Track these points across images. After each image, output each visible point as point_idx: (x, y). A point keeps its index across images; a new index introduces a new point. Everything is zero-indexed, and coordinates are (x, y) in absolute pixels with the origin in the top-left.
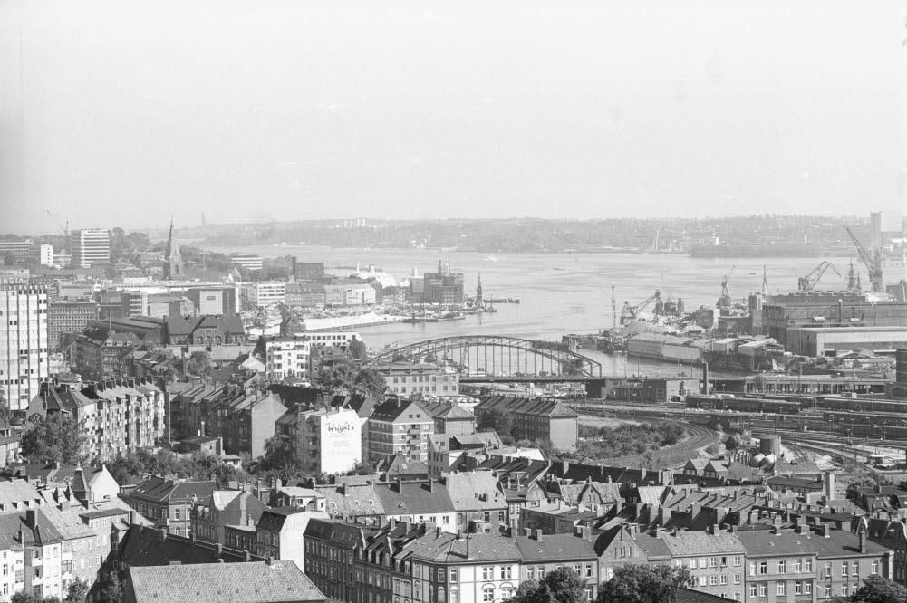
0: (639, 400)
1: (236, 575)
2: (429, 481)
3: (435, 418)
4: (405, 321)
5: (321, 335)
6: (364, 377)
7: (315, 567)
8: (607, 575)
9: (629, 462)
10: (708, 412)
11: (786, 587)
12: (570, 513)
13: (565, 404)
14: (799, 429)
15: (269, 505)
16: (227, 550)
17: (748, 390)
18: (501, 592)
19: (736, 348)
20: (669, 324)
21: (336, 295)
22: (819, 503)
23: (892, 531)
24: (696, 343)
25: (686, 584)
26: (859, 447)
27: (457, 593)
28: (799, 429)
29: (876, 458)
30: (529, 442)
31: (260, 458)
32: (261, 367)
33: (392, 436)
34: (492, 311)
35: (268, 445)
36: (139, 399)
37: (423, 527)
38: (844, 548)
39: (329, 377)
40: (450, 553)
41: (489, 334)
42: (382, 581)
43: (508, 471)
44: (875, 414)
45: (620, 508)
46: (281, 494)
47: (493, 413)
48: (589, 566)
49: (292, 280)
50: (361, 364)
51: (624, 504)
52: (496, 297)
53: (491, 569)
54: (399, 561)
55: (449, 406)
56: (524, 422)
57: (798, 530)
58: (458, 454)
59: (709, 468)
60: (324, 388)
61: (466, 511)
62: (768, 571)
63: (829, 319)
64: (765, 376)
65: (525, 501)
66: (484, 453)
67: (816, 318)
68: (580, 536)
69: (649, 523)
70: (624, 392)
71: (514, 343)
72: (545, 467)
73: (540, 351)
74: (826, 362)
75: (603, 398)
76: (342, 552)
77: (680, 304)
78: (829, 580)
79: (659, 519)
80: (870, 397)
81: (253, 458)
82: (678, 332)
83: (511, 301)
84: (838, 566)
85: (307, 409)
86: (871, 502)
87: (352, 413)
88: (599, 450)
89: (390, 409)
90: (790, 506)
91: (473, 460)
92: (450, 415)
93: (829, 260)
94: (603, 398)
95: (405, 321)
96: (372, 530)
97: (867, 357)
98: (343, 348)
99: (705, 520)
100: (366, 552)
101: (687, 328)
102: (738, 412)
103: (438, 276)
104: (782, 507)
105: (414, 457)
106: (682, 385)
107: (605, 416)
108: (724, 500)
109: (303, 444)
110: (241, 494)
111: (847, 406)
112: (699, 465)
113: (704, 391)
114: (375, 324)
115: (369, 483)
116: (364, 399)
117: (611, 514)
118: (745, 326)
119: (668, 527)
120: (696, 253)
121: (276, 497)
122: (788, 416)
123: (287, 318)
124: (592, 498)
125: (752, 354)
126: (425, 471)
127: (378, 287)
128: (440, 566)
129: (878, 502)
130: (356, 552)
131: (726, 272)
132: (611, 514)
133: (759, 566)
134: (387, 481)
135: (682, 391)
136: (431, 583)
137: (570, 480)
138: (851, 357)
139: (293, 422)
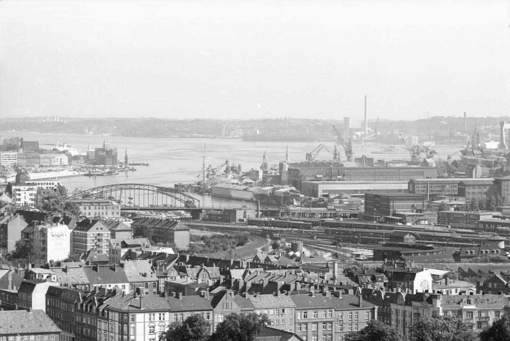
0: (221, 221)
1: (5, 317)
2: (112, 265)
3: (110, 230)
4: (85, 175)
5: (40, 182)
6: (68, 206)
7: (51, 311)
8: (220, 319)
9: (220, 255)
10: (260, 228)
11: (318, 326)
12: (193, 284)
13: (184, 223)
14: (312, 238)
15: (24, 278)
16: (4, 303)
17: (281, 216)
18: (159, 328)
19: (273, 192)
20: (234, 178)
21: (45, 160)
22: (331, 279)
23: (375, 295)
24: (251, 189)
25: (266, 324)
26: (347, 248)
27: (134, 328)
28: (312, 238)
29: (356, 255)
30: (163, 244)
31: (12, 251)
32: (9, 200)
33: (86, 240)
34: (133, 170)
35: (17, 244)
37: (115, 291)
38: (350, 304)
39: (50, 206)
40: (130, 306)
41: (138, 183)
42: (91, 322)
43: (157, 260)
44: (354, 230)
45: (222, 281)
46: (32, 272)
47: (142, 227)
48: (208, 314)
49: (21, 151)
50: (65, 199)
51: (224, 279)
52: (135, 162)
53: (154, 315)
54: (101, 310)
55: (118, 224)
56: (159, 232)
57: (324, 294)
58: (126, 250)
59: (267, 259)
60: (48, 212)
61: (135, 282)
62: (308, 317)
63: (325, 176)
64: (291, 208)
65: (167, 277)
66: (141, 250)
67: (318, 176)
68: (203, 296)
69: (240, 291)
70: (213, 216)
71: (151, 188)
72: (176, 258)
73: (166, 192)
74: (324, 201)
75: (201, 219)
76: (68, 305)
77: (239, 167)
78: (341, 322)
79: (244, 289)
80: (351, 220)
81: (9, 251)
82: (239, 183)
83: (144, 165)
84: (347, 314)
85: (40, 224)
86: (361, 279)
87: (65, 227)
88: (201, 249)
89: (86, 225)
90: (316, 281)
91: (135, 254)
92: (118, 228)
93: (322, 143)
94: (201, 219)
95: (85, 175)
96: (86, 292)
97: (347, 198)
98: (55, 190)
99: (271, 289)
100: (82, 305)
101: (245, 181)
102: (277, 228)
103: (103, 150)
104: (312, 281)
105: (99, 252)
106: (245, 213)
107: (203, 230)
108: (281, 277)
109: (37, 244)
110: (8, 272)
111: (338, 225)
112: (262, 257)
113: (257, 216)
114: (68, 177)
115: (81, 266)
116: (71, 219)
117: (217, 284)
118: (277, 180)
119: (250, 292)
120: (246, 138)
121: (28, 274)
122: (305, 230)
123: (20, 172)
124: (205, 275)
125: (282, 195)
126: (107, 260)
127: (69, 156)
128: (125, 313)
130: (76, 305)
131: (264, 149)
132: (217, 284)
133: (303, 314)
134: (90, 265)
135: (244, 217)
136: (119, 322)
137: (190, 265)
138: (338, 198)
139: (31, 232)
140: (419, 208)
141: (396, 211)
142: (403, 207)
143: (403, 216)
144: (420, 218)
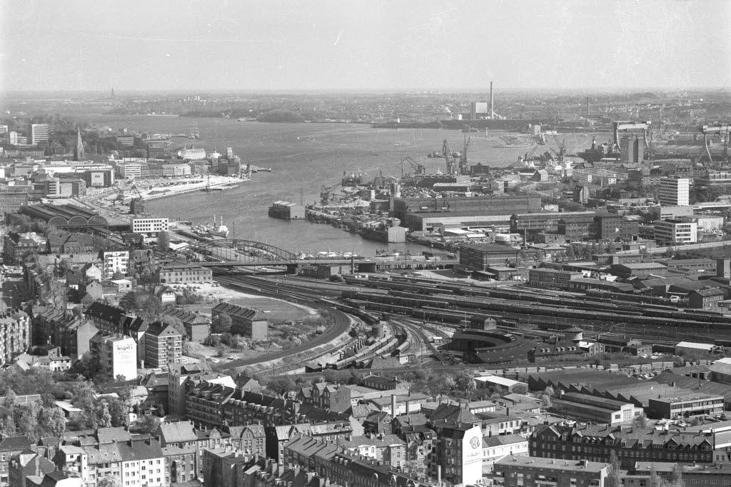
36: (13, 325)
58: (185, 377)
65: (209, 439)
92: (195, 322)
116: (142, 321)
129: (412, 437)
140: (512, 262)
141: (489, 266)
142: (498, 261)
143: (496, 272)
144: (513, 273)
